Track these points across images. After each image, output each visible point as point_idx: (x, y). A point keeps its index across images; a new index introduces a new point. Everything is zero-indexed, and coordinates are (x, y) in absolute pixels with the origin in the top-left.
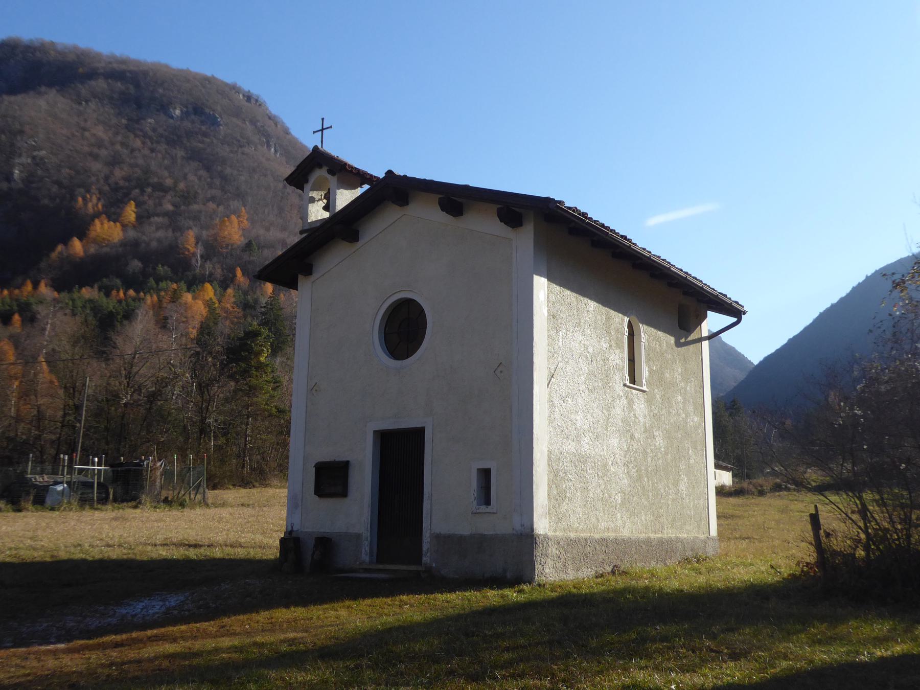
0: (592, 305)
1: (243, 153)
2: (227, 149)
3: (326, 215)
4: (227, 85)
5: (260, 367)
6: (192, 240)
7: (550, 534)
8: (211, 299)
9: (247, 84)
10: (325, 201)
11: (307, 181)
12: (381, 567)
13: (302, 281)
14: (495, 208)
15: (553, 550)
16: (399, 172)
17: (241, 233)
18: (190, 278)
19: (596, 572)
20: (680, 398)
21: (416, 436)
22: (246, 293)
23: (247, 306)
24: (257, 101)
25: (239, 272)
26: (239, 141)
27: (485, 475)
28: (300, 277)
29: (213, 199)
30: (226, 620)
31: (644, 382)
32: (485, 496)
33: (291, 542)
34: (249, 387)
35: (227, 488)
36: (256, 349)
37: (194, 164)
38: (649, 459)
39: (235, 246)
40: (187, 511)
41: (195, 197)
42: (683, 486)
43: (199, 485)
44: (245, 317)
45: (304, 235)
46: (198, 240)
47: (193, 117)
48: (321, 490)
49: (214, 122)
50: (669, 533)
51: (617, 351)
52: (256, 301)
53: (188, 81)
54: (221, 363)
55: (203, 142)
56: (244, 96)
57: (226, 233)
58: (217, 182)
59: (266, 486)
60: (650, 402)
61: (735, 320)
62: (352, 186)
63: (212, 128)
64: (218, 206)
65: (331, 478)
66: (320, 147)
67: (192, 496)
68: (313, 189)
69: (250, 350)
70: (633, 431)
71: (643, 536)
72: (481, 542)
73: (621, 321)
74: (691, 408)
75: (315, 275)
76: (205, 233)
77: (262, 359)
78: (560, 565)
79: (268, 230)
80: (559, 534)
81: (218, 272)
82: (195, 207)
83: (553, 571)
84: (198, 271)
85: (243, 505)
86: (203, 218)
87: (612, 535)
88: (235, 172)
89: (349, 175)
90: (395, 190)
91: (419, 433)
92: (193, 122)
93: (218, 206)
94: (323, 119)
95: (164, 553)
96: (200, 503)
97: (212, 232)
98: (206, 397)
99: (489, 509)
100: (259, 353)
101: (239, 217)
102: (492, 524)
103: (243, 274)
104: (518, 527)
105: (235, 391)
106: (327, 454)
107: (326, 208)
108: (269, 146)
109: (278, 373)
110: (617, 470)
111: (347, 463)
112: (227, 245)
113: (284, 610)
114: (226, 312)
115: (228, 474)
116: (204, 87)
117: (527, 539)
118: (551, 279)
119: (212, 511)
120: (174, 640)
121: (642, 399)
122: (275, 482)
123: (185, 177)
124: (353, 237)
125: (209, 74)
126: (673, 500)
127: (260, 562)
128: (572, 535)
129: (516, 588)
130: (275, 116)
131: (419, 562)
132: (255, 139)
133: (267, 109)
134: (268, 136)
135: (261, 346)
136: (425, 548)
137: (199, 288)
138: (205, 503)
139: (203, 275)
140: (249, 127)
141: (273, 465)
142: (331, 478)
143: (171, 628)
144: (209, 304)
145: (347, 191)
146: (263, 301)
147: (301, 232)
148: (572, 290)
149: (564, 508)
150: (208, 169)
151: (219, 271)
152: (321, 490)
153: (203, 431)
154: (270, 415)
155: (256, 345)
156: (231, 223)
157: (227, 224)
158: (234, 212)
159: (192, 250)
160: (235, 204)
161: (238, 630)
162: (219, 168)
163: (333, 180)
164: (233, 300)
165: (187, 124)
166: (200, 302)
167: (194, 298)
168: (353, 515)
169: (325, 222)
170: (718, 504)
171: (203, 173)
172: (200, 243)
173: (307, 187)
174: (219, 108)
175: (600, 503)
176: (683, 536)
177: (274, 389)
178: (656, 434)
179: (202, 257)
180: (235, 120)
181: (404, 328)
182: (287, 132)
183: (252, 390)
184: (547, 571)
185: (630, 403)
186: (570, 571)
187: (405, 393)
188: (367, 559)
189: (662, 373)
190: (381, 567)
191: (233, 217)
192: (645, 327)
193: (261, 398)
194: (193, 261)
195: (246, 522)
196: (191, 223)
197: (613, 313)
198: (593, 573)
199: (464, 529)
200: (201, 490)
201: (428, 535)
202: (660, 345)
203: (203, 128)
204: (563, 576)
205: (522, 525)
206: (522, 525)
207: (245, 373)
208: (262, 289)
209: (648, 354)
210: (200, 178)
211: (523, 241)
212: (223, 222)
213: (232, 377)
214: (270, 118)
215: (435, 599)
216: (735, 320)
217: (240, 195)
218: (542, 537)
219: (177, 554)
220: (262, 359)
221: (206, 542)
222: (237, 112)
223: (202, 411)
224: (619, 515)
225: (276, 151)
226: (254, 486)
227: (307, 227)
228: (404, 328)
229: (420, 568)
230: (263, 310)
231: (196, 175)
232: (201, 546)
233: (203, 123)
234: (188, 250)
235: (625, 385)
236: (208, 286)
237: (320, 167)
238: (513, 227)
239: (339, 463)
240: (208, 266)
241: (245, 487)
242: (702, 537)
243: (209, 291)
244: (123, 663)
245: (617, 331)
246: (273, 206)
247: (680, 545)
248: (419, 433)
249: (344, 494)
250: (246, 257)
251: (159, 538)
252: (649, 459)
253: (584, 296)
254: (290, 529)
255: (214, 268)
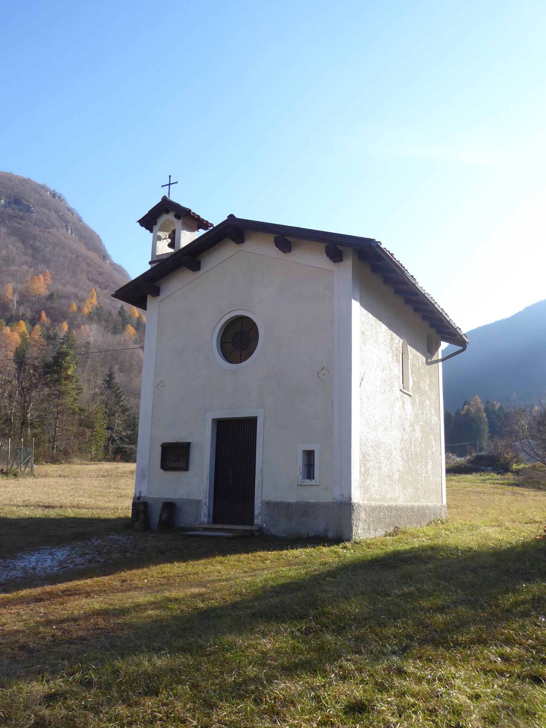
0: (383, 328)
1: (49, 233)
2: (38, 229)
3: (172, 250)
4: (39, 185)
5: (68, 378)
6: (10, 291)
7: (361, 502)
8: (24, 332)
9: (53, 186)
10: (169, 241)
11: (156, 223)
12: (213, 526)
13: (151, 302)
14: (323, 246)
15: (363, 516)
16: (238, 216)
17: (46, 287)
18: (8, 317)
19: (386, 532)
20: (428, 403)
21: (250, 423)
22: (48, 329)
23: (50, 338)
24: (60, 197)
25: (43, 314)
26: (46, 224)
27: (309, 455)
28: (149, 297)
29: (26, 263)
30: (126, 574)
31: (410, 388)
32: (309, 470)
33: (140, 505)
34: (59, 392)
35: (42, 464)
36: (65, 365)
37: (13, 238)
38: (413, 447)
39: (41, 296)
40: (21, 480)
41: (13, 261)
42: (429, 467)
43: (28, 461)
44: (48, 345)
45: (154, 265)
46: (15, 290)
47: (14, 206)
48: (165, 466)
49: (28, 210)
50: (423, 503)
51: (397, 364)
52: (56, 335)
53: (11, 180)
54: (40, 374)
55: (20, 224)
56: (50, 193)
57: (35, 287)
58: (30, 251)
59: (70, 463)
60: (413, 403)
61: (461, 348)
62: (192, 229)
63: (27, 214)
64: (30, 268)
65: (175, 456)
66: (168, 196)
67: (22, 469)
68: (161, 230)
69: (60, 366)
70: (405, 426)
71: (409, 504)
72: (306, 509)
73: (398, 341)
74: (433, 411)
75: (162, 296)
76: (20, 286)
77: (69, 373)
78: (366, 527)
79: (65, 286)
80: (366, 502)
81: (29, 314)
82: (13, 268)
83: (368, 534)
84: (14, 312)
85: (60, 476)
86: (18, 276)
87: (393, 503)
88: (42, 246)
89: (193, 221)
90: (236, 230)
91: (252, 422)
92: (13, 209)
93: (30, 268)
94: (170, 176)
95: (28, 513)
96: (28, 474)
97: (25, 286)
98: (28, 399)
99: (313, 482)
100: (67, 369)
101: (44, 276)
102: (316, 493)
103: (47, 316)
104: (338, 497)
105: (49, 395)
106: (172, 437)
107: (171, 245)
108: (67, 229)
109: (80, 383)
110: (396, 454)
111: (189, 444)
112: (36, 296)
113: (169, 565)
114: (34, 341)
115: (43, 453)
116: (22, 186)
117: (346, 507)
118: (362, 304)
119: (41, 480)
120: (88, 595)
121: (409, 401)
122: (76, 460)
123: (6, 247)
124: (196, 267)
125: (26, 177)
126: (425, 477)
127: (106, 520)
128: (373, 504)
129: (341, 546)
130: (72, 209)
131: (251, 523)
132: (58, 223)
133: (67, 204)
134: (66, 222)
135: (69, 363)
136: (256, 512)
137: (15, 324)
138: (32, 474)
139: (18, 315)
140: (53, 215)
141: (76, 448)
142: (175, 456)
143: (78, 583)
144: (22, 335)
145: (188, 233)
146: (62, 335)
147: (150, 263)
148: (373, 315)
149: (368, 483)
150: (23, 242)
151: (30, 313)
152: (165, 466)
153: (24, 423)
154: (74, 413)
155: (65, 362)
156: (39, 279)
157: (36, 280)
158: (41, 273)
159: (10, 297)
160: (41, 267)
161: (140, 584)
162: (31, 242)
163: (178, 224)
164: (40, 333)
165: (9, 211)
166: (16, 334)
167: (12, 331)
168: (195, 485)
169: (171, 257)
170: (447, 480)
171: (20, 245)
172: (16, 293)
173: (156, 228)
174: (32, 201)
175: (387, 479)
176: (430, 504)
177: (77, 394)
178: (416, 428)
179: (17, 302)
180: (43, 209)
181: (239, 339)
182: (80, 220)
183: (61, 394)
184: (359, 531)
185: (404, 403)
186: (372, 532)
187: (239, 391)
188: (206, 520)
189: (419, 384)
190: (213, 526)
191: (41, 276)
192: (411, 348)
193: (68, 400)
194: (11, 305)
195: (97, 489)
196: (10, 279)
197: (395, 335)
198: (384, 532)
199: (291, 498)
200: (30, 464)
201: (259, 501)
202: (418, 362)
203: (21, 214)
204: (368, 535)
205: (342, 495)
206: (342, 495)
207: (58, 381)
208: (59, 326)
209: (412, 368)
210: (17, 248)
211: (345, 272)
212: (33, 279)
213: (46, 384)
214: (68, 210)
215: (286, 555)
216: (461, 348)
217: (45, 261)
218: (356, 505)
219: (39, 513)
220: (69, 373)
221: (58, 504)
222: (45, 204)
223: (24, 409)
224: (397, 488)
225: (72, 232)
226: (61, 463)
227: (156, 259)
228: (239, 339)
229: (254, 528)
230: (61, 340)
231: (14, 246)
232: (54, 507)
233: (20, 210)
234: (8, 298)
235: (401, 390)
236: (22, 322)
237: (167, 212)
238: (334, 262)
239: (182, 444)
240: (22, 309)
241: (54, 464)
242: (439, 505)
243: (23, 326)
244: (62, 621)
245: (397, 349)
246: (69, 270)
247: (428, 511)
248: (252, 422)
249: (186, 468)
250: (49, 304)
251: (19, 500)
252: (413, 447)
253: (380, 320)
254: (138, 495)
255: (26, 310)
